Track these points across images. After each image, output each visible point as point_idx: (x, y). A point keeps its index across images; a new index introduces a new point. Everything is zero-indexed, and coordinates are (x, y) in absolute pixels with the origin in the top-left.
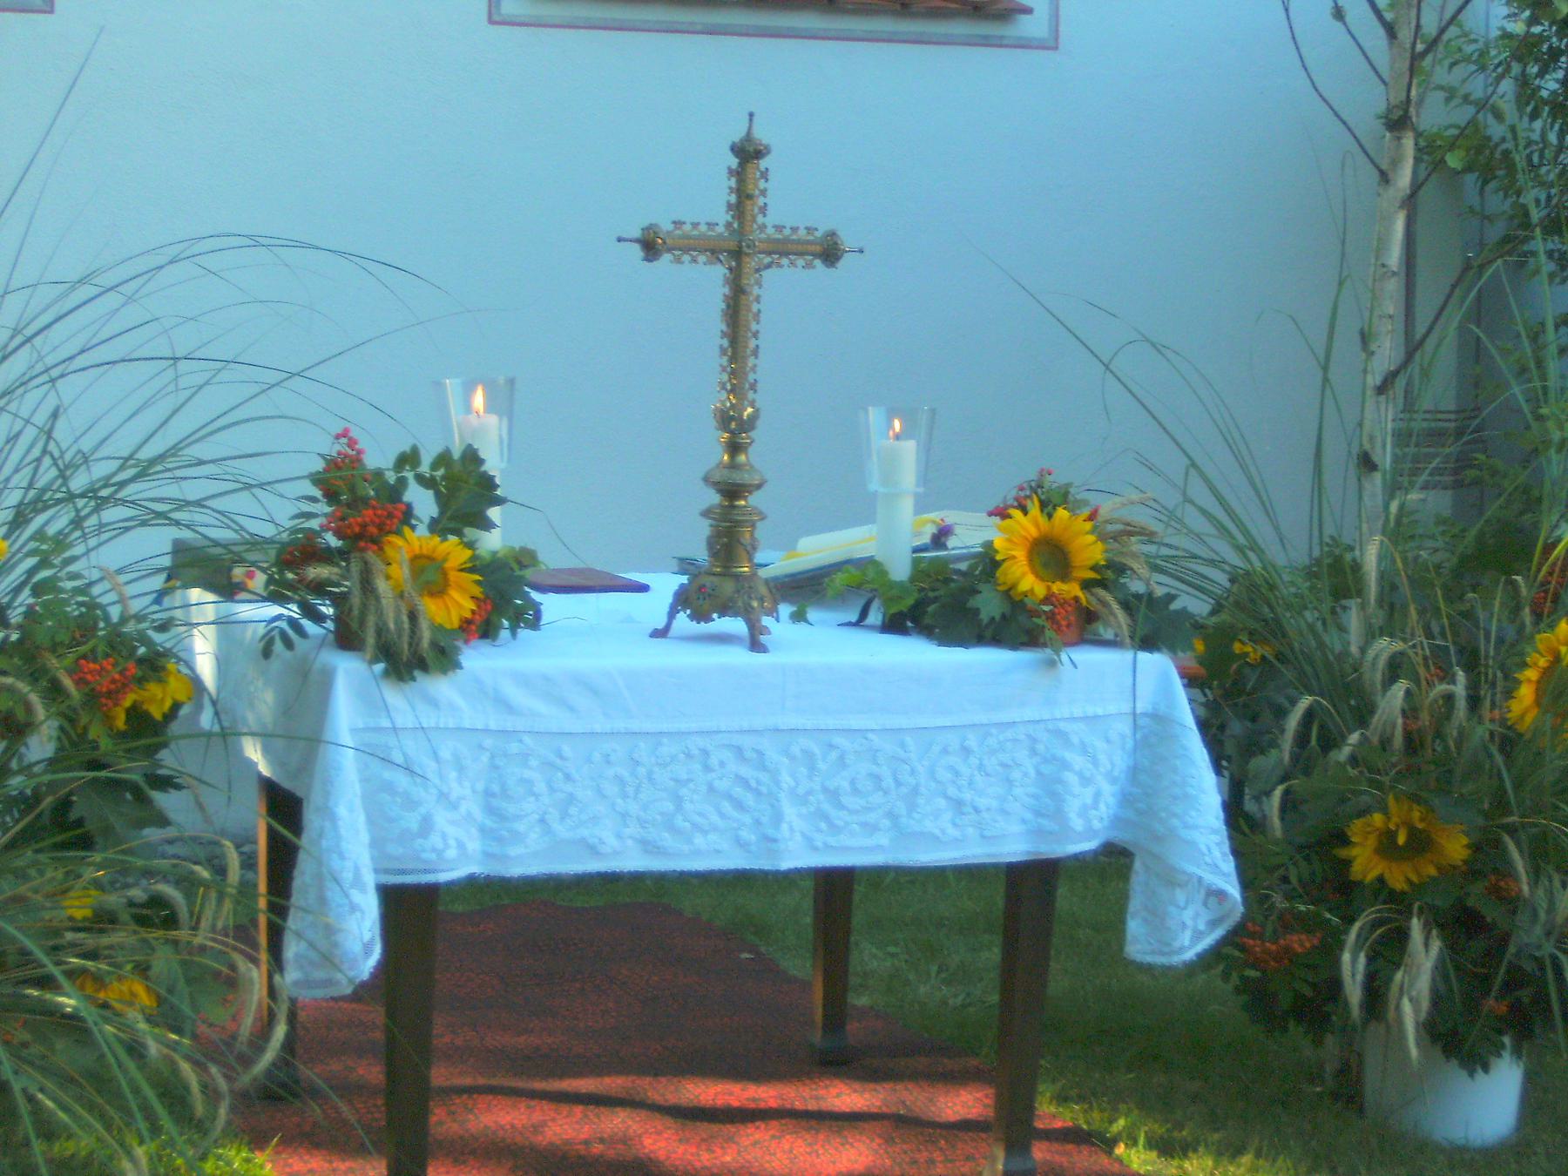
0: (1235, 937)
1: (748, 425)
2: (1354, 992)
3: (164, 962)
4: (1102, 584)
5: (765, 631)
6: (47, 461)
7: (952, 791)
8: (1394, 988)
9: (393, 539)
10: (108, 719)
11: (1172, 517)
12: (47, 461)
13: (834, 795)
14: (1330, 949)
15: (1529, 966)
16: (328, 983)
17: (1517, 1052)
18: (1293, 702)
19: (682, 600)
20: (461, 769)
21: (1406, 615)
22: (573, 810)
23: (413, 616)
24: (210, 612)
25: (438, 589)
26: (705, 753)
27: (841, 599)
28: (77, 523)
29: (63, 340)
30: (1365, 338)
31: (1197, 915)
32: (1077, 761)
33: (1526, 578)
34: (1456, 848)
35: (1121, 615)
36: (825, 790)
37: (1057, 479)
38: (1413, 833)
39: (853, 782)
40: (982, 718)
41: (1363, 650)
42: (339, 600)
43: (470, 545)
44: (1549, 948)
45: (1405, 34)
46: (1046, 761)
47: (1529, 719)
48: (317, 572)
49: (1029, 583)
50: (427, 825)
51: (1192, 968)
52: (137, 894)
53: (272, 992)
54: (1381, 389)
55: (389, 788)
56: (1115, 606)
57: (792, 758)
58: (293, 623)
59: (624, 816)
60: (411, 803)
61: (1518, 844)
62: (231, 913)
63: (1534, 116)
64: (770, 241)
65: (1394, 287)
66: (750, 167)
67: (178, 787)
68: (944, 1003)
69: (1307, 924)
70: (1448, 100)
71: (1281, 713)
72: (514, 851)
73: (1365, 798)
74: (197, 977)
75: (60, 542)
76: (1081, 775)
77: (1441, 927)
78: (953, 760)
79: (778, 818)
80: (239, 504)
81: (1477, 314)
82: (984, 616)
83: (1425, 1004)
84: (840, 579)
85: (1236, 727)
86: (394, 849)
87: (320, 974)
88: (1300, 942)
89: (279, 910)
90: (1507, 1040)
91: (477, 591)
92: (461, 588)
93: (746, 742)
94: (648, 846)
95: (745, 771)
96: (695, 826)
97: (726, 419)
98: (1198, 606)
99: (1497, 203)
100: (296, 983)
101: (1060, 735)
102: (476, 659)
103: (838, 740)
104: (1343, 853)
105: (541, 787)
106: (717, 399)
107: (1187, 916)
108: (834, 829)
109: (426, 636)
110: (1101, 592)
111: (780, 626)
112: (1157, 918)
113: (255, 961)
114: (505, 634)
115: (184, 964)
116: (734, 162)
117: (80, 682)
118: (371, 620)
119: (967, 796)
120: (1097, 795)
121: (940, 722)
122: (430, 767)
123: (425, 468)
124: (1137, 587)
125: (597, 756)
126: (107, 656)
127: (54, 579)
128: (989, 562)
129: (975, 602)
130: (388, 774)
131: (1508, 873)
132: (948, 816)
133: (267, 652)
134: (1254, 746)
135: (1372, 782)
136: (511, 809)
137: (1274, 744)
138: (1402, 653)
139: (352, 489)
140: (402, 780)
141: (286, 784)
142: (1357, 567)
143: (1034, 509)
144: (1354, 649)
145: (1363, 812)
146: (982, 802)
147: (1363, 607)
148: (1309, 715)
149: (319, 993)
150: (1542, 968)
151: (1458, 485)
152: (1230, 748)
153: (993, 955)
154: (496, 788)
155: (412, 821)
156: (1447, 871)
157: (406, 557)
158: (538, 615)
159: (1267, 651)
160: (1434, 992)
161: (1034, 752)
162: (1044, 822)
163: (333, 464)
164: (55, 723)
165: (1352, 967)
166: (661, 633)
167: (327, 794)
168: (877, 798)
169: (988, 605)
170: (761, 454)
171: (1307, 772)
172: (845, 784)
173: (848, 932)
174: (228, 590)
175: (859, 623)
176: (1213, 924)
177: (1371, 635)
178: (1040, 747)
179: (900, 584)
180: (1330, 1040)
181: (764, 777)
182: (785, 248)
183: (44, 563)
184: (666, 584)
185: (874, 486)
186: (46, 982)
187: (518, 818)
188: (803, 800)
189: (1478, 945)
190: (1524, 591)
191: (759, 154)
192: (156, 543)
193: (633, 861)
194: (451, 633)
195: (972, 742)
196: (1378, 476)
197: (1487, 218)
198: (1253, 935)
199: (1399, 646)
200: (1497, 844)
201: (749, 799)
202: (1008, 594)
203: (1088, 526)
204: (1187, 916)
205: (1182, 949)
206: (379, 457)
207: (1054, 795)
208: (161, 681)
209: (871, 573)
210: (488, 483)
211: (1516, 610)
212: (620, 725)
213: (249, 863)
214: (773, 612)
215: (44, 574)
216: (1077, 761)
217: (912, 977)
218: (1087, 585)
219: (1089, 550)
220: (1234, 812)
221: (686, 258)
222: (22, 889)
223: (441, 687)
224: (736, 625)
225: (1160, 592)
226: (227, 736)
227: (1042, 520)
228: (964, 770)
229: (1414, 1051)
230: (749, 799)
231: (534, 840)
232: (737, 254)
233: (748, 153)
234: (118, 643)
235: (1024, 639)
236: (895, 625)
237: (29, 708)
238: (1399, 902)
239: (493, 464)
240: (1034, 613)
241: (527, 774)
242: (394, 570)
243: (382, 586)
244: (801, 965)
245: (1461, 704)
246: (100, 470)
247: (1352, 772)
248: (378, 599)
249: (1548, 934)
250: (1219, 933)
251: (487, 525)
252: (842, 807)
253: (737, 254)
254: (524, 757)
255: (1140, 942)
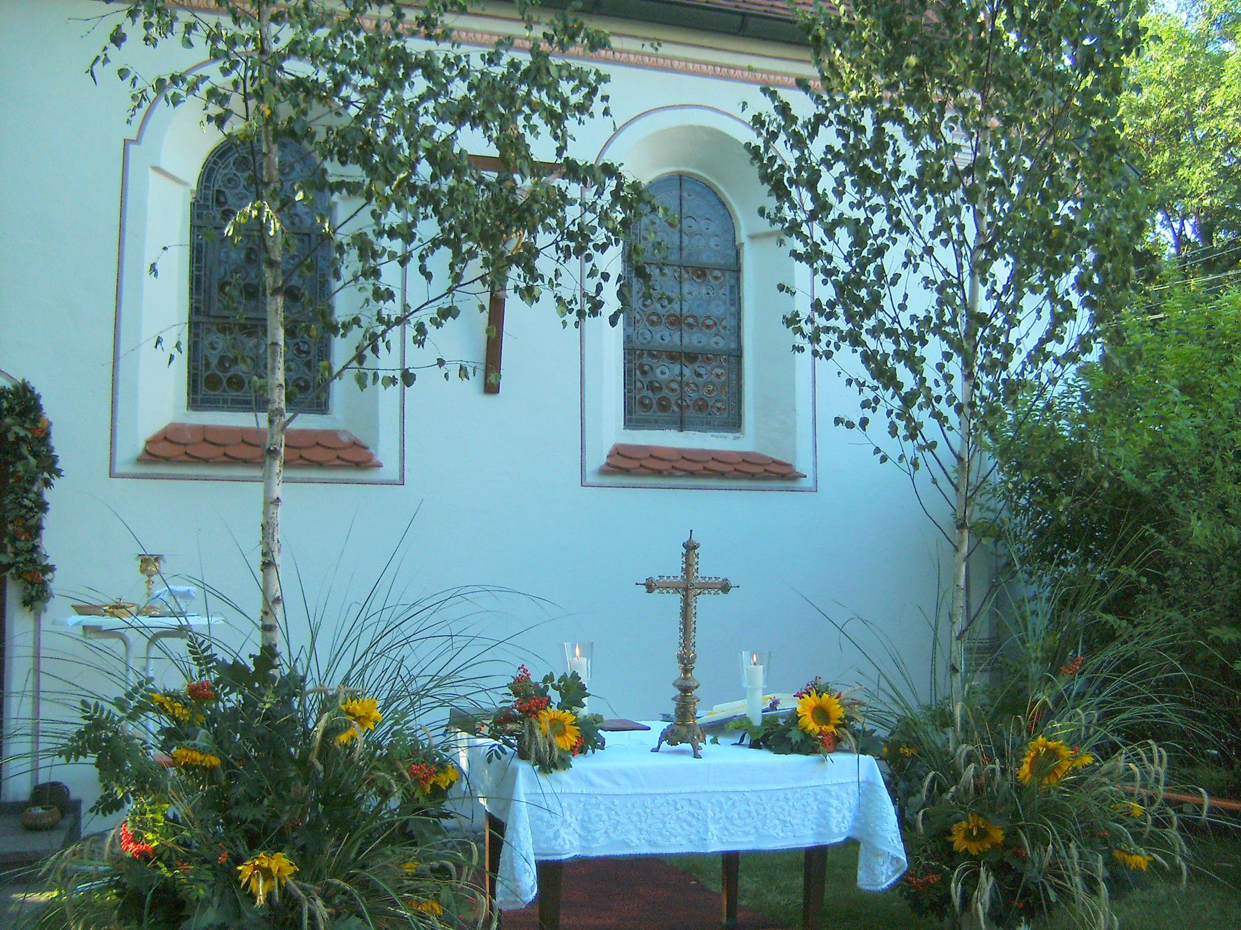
0: (905, 879)
1: (691, 661)
2: (956, 900)
3: (446, 894)
4: (844, 726)
5: (700, 748)
6: (399, 679)
7: (781, 817)
8: (974, 900)
9: (542, 711)
10: (423, 790)
11: (872, 695)
12: (399, 679)
13: (730, 819)
14: (946, 881)
15: (1032, 887)
16: (515, 902)
17: (1027, 923)
18: (927, 774)
19: (666, 736)
20: (571, 811)
21: (973, 733)
22: (619, 828)
23: (551, 746)
24: (465, 743)
25: (561, 733)
26: (676, 803)
27: (731, 733)
28: (412, 704)
29: (408, 628)
30: (951, 616)
31: (888, 868)
32: (835, 802)
33: (1024, 717)
34: (998, 836)
35: (852, 739)
36: (727, 817)
37: (822, 682)
38: (979, 829)
39: (739, 814)
40: (794, 785)
41: (955, 750)
42: (519, 738)
43: (575, 714)
44: (1040, 879)
45: (963, 489)
46: (821, 803)
47: (1028, 778)
48: (510, 727)
49: (812, 726)
50: (557, 835)
51: (885, 891)
52: (435, 864)
53: (491, 907)
54: (958, 638)
55: (541, 819)
56: (849, 735)
57: (712, 804)
58: (500, 747)
59: (641, 830)
60: (550, 826)
61: (1025, 833)
62: (628, 296)
63: (1016, 516)
64: (699, 583)
65: (962, 594)
66: (691, 553)
67: (452, 817)
68: (779, 903)
69: (937, 870)
70: (981, 509)
71: (921, 778)
72: (593, 846)
73: (959, 815)
74: (459, 900)
75: (404, 714)
76: (836, 808)
77: (994, 870)
78: (781, 803)
79: (707, 830)
80: (481, 697)
81: (997, 604)
82: (793, 741)
83: (987, 906)
84: (731, 725)
85: (902, 785)
86: (543, 845)
87: (511, 899)
88: (934, 879)
89: (494, 866)
90: (1023, 918)
91: (578, 734)
92: (571, 733)
93: (693, 797)
94: (652, 843)
95: (692, 810)
96: (671, 834)
97: (681, 659)
98: (882, 733)
99: (1001, 551)
100: (501, 902)
101: (828, 792)
102: (578, 762)
103: (732, 796)
104: (950, 839)
105: (605, 817)
106: (678, 650)
107: (884, 869)
108: (731, 834)
109: (556, 753)
110: (843, 730)
111: (707, 747)
112: (871, 870)
113: (484, 895)
114: (590, 751)
115: (455, 896)
116: (684, 551)
117: (412, 774)
118: (533, 747)
119: (788, 819)
120: (844, 817)
121: (775, 787)
122: (558, 810)
123: (556, 682)
124: (858, 726)
125: (629, 804)
126: (423, 763)
127: (401, 730)
128: (794, 717)
129: (790, 735)
130: (540, 813)
131: (1021, 846)
132: (780, 827)
133: (489, 761)
134: (910, 793)
135: (961, 808)
136: (592, 827)
137: (919, 791)
138: (972, 751)
139: (525, 692)
140: (546, 815)
141: (496, 816)
142: (951, 714)
143: (813, 693)
144: (951, 749)
145: (957, 821)
146: (794, 822)
147: (954, 731)
148: (934, 778)
149: (511, 907)
150: (1037, 887)
151: (992, 670)
152: (900, 793)
153: (800, 881)
154: (586, 818)
155: (551, 833)
156: (994, 846)
157: (548, 719)
158: (603, 743)
159: (914, 751)
160: (991, 897)
161: (816, 799)
162: (821, 829)
163: (518, 680)
164: (401, 791)
165: (956, 890)
166: (656, 750)
167: (514, 822)
168: (749, 821)
169: (795, 736)
170: (697, 674)
171: (933, 804)
172: (736, 815)
173: (737, 872)
174: (474, 732)
175: (740, 744)
176: (894, 872)
177: (958, 743)
178: (819, 797)
179: (757, 727)
180: (946, 920)
181: (700, 812)
182: (707, 587)
183: (397, 723)
184: (659, 727)
185: (745, 685)
186: (394, 904)
187: (595, 831)
188: (717, 822)
189: (1010, 878)
190: (1023, 723)
191: (695, 548)
192: (443, 714)
193: (645, 850)
194: (567, 752)
195: (790, 796)
196: (959, 675)
197: (998, 556)
198: (912, 876)
199: (970, 748)
200: (1016, 833)
201: (694, 822)
202: (803, 731)
203: (837, 701)
204: (884, 869)
205: (882, 883)
206: (536, 677)
207: (825, 818)
208: (445, 772)
209: (745, 723)
210: (583, 688)
211: (1020, 731)
212: (639, 791)
213: (481, 852)
214: (704, 741)
215: (396, 728)
216: (835, 802)
217: (764, 891)
218: (837, 726)
219: (837, 712)
220: (905, 824)
221: (665, 591)
222: (386, 863)
223: (562, 775)
224: (688, 746)
225: (868, 728)
226: (473, 797)
227: (817, 699)
228: (787, 808)
229: (983, 927)
230: (694, 822)
231: (602, 840)
232: (686, 589)
233: (690, 547)
234: (428, 757)
235: (810, 750)
236: (755, 745)
237: (390, 785)
238: (975, 860)
239: (585, 680)
240: (816, 739)
241: (599, 812)
242: (543, 726)
243: (538, 732)
244: (717, 887)
245: (998, 773)
246: (421, 682)
247: (953, 804)
248: (536, 738)
249: (1039, 873)
250: (898, 875)
251: (583, 706)
252: (734, 825)
253: (686, 589)
254: (597, 806)
255: (864, 881)
